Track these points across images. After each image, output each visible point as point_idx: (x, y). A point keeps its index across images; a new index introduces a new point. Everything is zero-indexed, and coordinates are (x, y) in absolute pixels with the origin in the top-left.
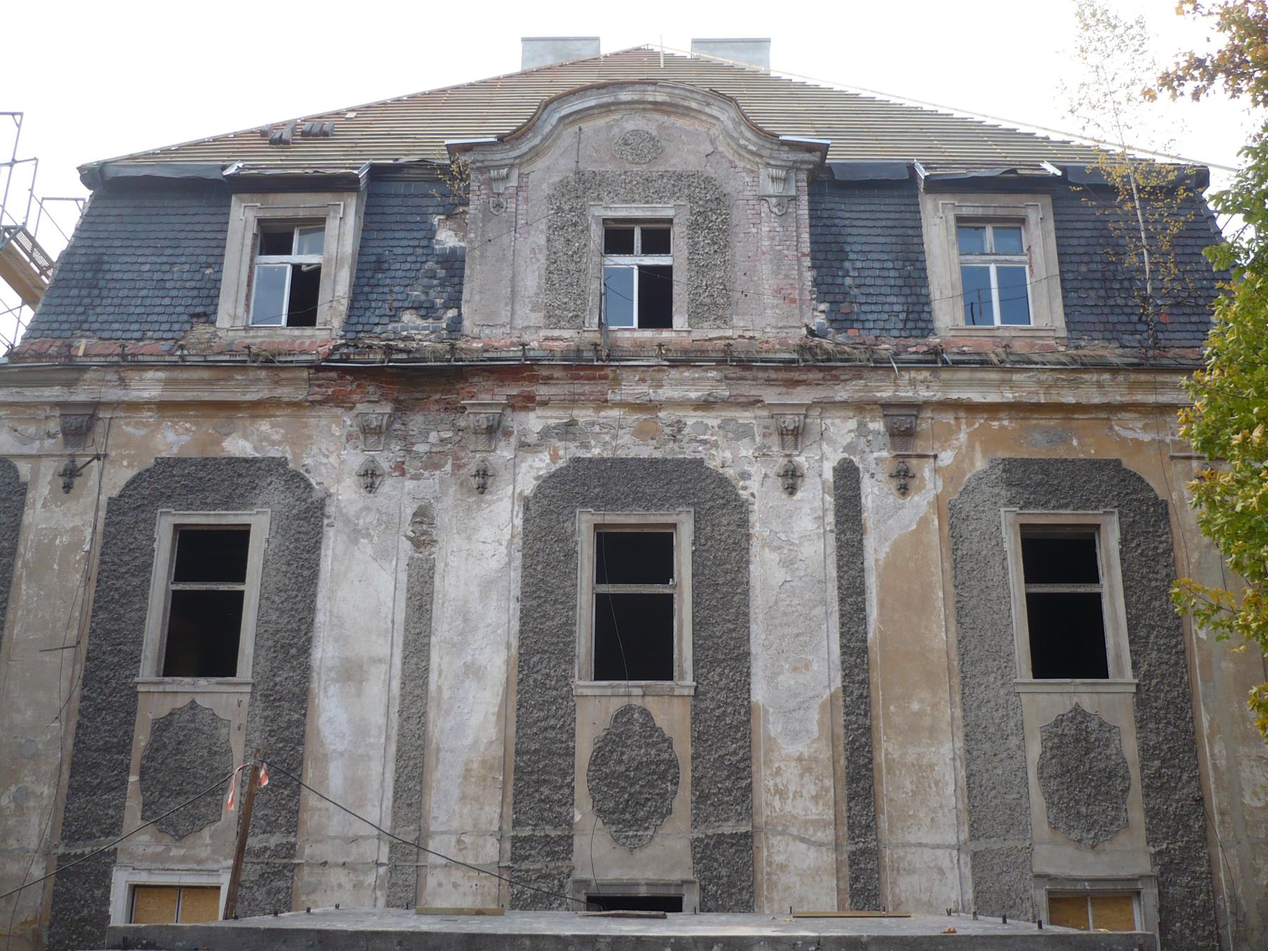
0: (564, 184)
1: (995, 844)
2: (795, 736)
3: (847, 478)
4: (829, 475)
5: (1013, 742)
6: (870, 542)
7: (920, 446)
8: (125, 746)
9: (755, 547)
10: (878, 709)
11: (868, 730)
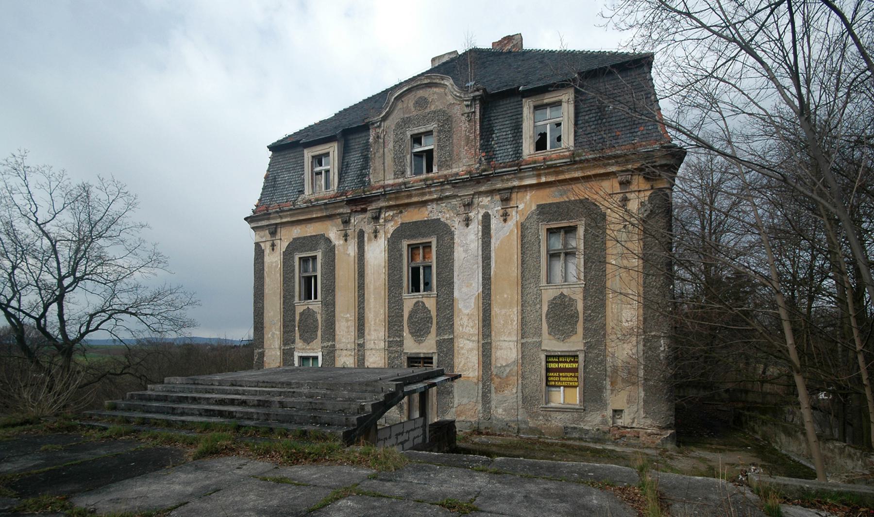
0: (398, 124)
1: (530, 340)
2: (467, 307)
3: (487, 218)
4: (480, 218)
5: (538, 306)
6: (493, 241)
7: (512, 204)
8: (294, 321)
9: (456, 246)
10: (493, 298)
11: (490, 305)
